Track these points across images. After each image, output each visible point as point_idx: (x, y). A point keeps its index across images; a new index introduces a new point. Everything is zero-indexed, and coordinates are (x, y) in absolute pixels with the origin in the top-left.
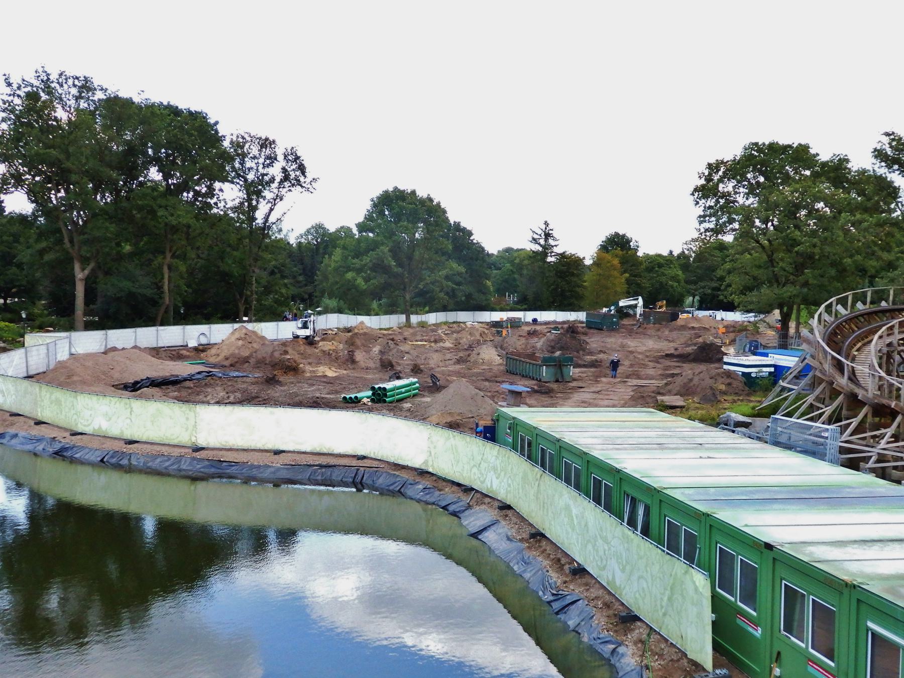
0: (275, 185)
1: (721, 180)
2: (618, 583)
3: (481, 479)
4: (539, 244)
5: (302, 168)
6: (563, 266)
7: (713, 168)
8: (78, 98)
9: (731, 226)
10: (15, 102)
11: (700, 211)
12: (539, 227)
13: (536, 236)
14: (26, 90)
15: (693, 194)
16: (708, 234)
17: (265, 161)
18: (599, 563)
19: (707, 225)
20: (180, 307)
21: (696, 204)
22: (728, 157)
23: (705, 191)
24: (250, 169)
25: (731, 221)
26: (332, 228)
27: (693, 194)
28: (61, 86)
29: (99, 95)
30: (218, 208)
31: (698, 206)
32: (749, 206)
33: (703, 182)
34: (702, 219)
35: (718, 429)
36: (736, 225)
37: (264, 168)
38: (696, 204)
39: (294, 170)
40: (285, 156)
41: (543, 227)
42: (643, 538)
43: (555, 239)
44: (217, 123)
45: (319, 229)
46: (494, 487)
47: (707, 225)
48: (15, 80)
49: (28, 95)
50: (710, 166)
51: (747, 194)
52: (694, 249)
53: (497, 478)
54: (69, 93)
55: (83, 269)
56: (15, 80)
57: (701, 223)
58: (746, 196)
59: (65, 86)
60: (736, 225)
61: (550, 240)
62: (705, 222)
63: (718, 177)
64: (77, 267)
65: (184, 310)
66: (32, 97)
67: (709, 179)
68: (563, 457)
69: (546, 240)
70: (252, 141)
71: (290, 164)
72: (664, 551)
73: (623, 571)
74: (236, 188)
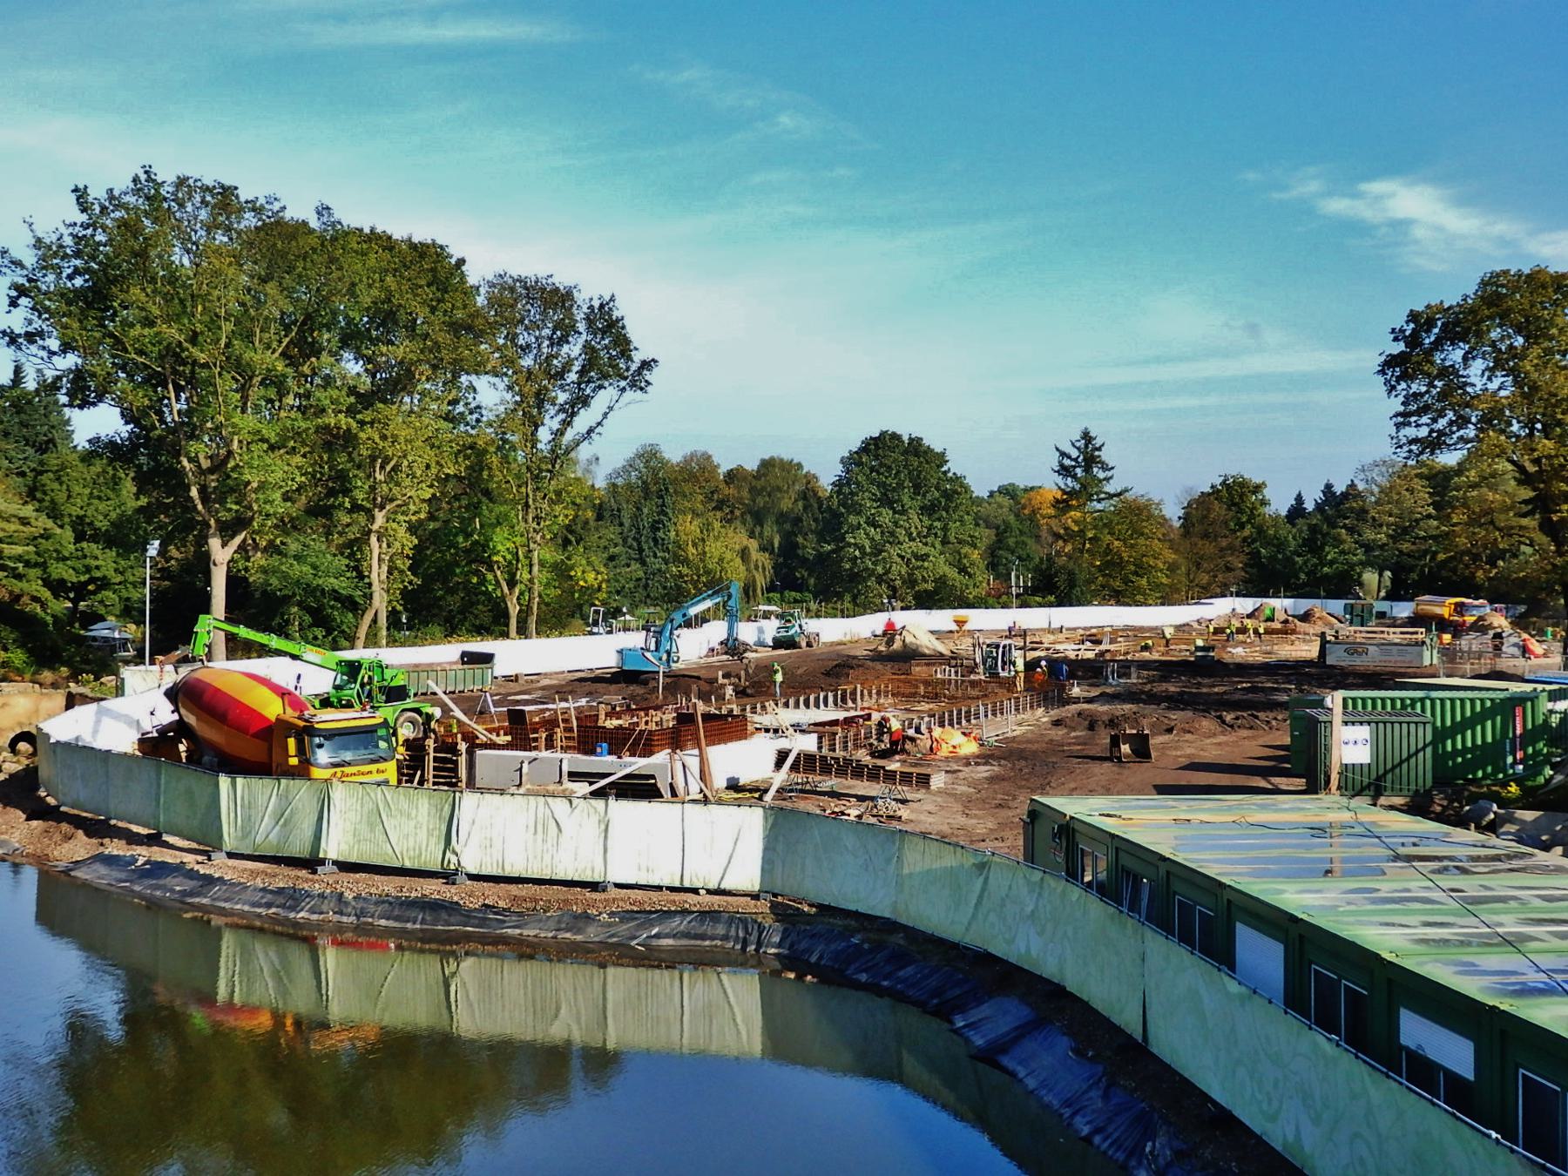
0: (572, 377)
1: (1437, 345)
2: (1307, 1149)
3: (1007, 936)
4: (1074, 477)
5: (623, 345)
6: (85, 229)
7: (1421, 321)
8: (210, 228)
9: (1462, 432)
10: (98, 238)
11: (1396, 404)
12: (1068, 437)
13: (1067, 462)
14: (118, 214)
15: (1382, 372)
16: (1414, 447)
17: (554, 333)
18: (1265, 1106)
19: (1411, 432)
20: (400, 612)
21: (1390, 392)
22: (1451, 300)
23: (1398, 367)
24: (526, 348)
25: (1462, 421)
26: (674, 454)
27: (1382, 372)
28: (182, 205)
29: (249, 220)
30: (467, 424)
31: (1394, 393)
32: (1495, 393)
33: (1400, 347)
34: (1403, 419)
35: (1501, 844)
36: (1470, 432)
37: (552, 345)
38: (1390, 392)
39: (606, 347)
40: (589, 321)
41: (607, 298)
42: (1357, 1057)
43: (1105, 467)
44: (461, 262)
45: (649, 456)
46: (1034, 953)
47: (1411, 432)
48: (97, 193)
49: (123, 224)
50: (1413, 316)
51: (1492, 370)
52: (1379, 479)
53: (1040, 934)
54: (196, 219)
55: (224, 545)
56: (97, 193)
57: (1398, 426)
58: (1487, 374)
59: (189, 208)
60: (1470, 432)
61: (1095, 470)
62: (1409, 424)
63: (1432, 339)
64: (215, 543)
65: (407, 618)
66: (128, 227)
67: (1413, 341)
68: (1175, 893)
69: (1088, 469)
70: (528, 296)
71: (599, 336)
72: (1401, 1084)
73: (1316, 1121)
74: (501, 384)
